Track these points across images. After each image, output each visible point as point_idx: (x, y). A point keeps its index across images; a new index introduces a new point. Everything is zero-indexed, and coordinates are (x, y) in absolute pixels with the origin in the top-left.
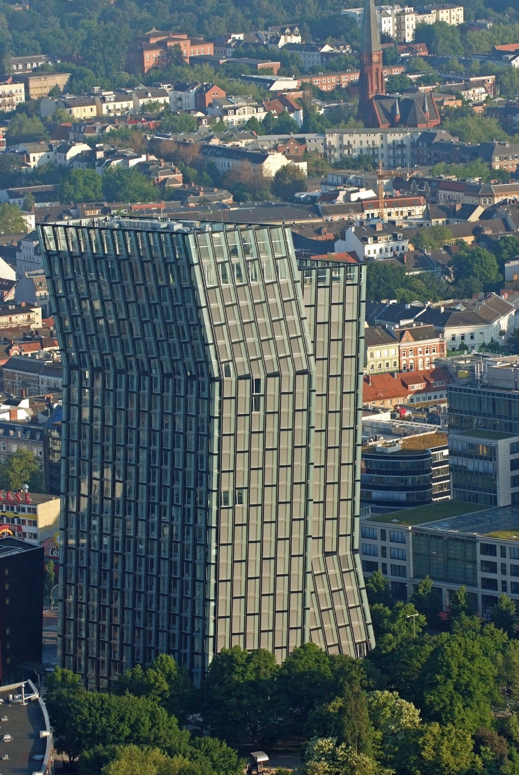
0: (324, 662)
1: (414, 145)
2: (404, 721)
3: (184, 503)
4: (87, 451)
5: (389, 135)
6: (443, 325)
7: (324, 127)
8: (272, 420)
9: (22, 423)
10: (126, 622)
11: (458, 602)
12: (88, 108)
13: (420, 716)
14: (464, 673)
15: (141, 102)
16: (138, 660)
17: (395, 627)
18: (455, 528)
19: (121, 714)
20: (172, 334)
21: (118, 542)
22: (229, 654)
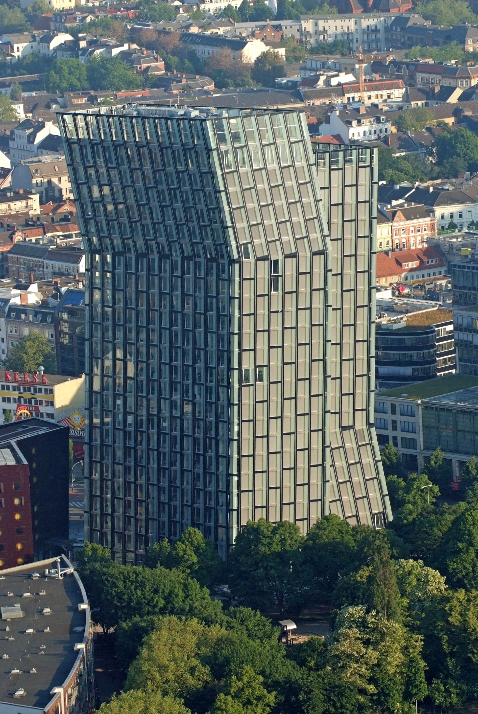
0: (347, 533)
1: (388, 29)
2: (431, 588)
3: (206, 381)
4: (110, 334)
5: (363, 20)
6: (432, 205)
7: (299, 14)
8: (290, 299)
9: (33, 306)
10: (151, 497)
11: (469, 472)
13: (445, 583)
16: (164, 534)
18: (463, 401)
19: (155, 586)
20: (191, 218)
21: (142, 420)
22: (255, 526)
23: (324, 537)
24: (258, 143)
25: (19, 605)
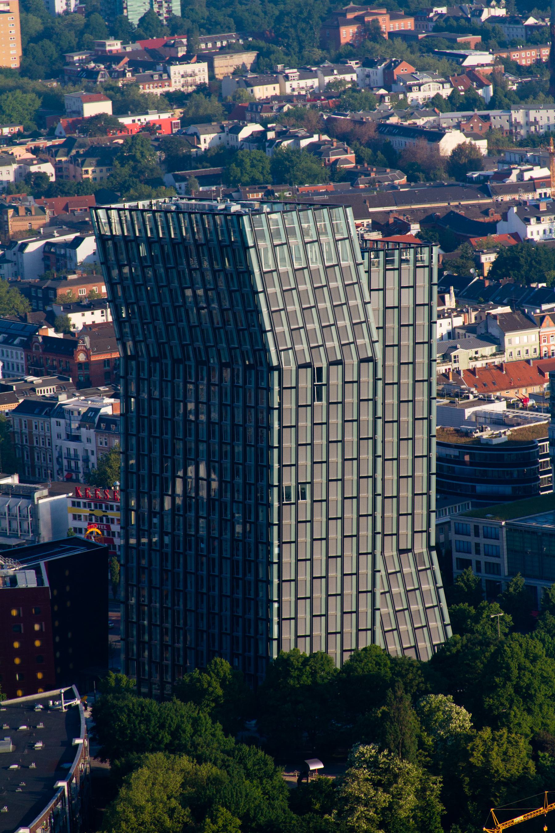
0: (385, 665)
12: (270, 87)
14: (524, 675)
15: (327, 79)
17: (479, 627)
19: (161, 721)
20: (228, 321)
23: (359, 669)
24: (299, 240)
25: (9, 739)
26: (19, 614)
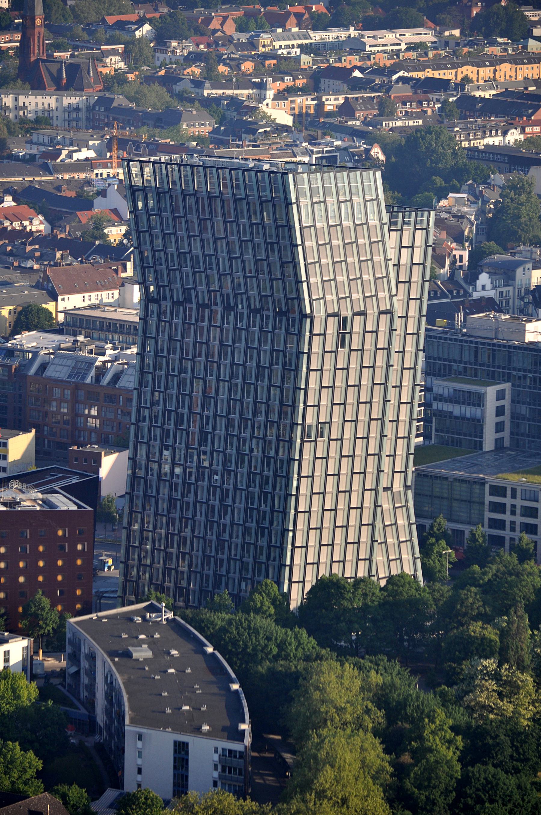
5: (64, 98)
26: (64, 535)
